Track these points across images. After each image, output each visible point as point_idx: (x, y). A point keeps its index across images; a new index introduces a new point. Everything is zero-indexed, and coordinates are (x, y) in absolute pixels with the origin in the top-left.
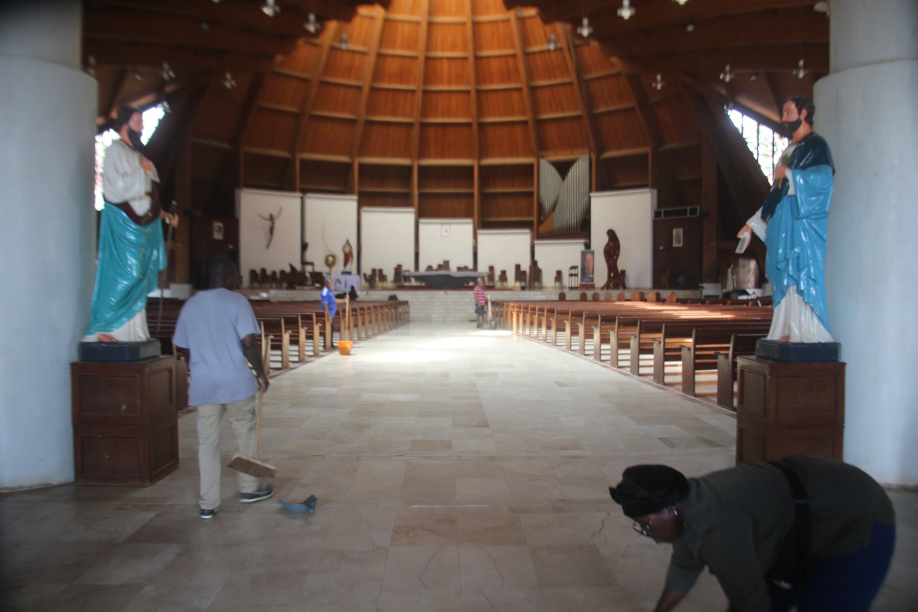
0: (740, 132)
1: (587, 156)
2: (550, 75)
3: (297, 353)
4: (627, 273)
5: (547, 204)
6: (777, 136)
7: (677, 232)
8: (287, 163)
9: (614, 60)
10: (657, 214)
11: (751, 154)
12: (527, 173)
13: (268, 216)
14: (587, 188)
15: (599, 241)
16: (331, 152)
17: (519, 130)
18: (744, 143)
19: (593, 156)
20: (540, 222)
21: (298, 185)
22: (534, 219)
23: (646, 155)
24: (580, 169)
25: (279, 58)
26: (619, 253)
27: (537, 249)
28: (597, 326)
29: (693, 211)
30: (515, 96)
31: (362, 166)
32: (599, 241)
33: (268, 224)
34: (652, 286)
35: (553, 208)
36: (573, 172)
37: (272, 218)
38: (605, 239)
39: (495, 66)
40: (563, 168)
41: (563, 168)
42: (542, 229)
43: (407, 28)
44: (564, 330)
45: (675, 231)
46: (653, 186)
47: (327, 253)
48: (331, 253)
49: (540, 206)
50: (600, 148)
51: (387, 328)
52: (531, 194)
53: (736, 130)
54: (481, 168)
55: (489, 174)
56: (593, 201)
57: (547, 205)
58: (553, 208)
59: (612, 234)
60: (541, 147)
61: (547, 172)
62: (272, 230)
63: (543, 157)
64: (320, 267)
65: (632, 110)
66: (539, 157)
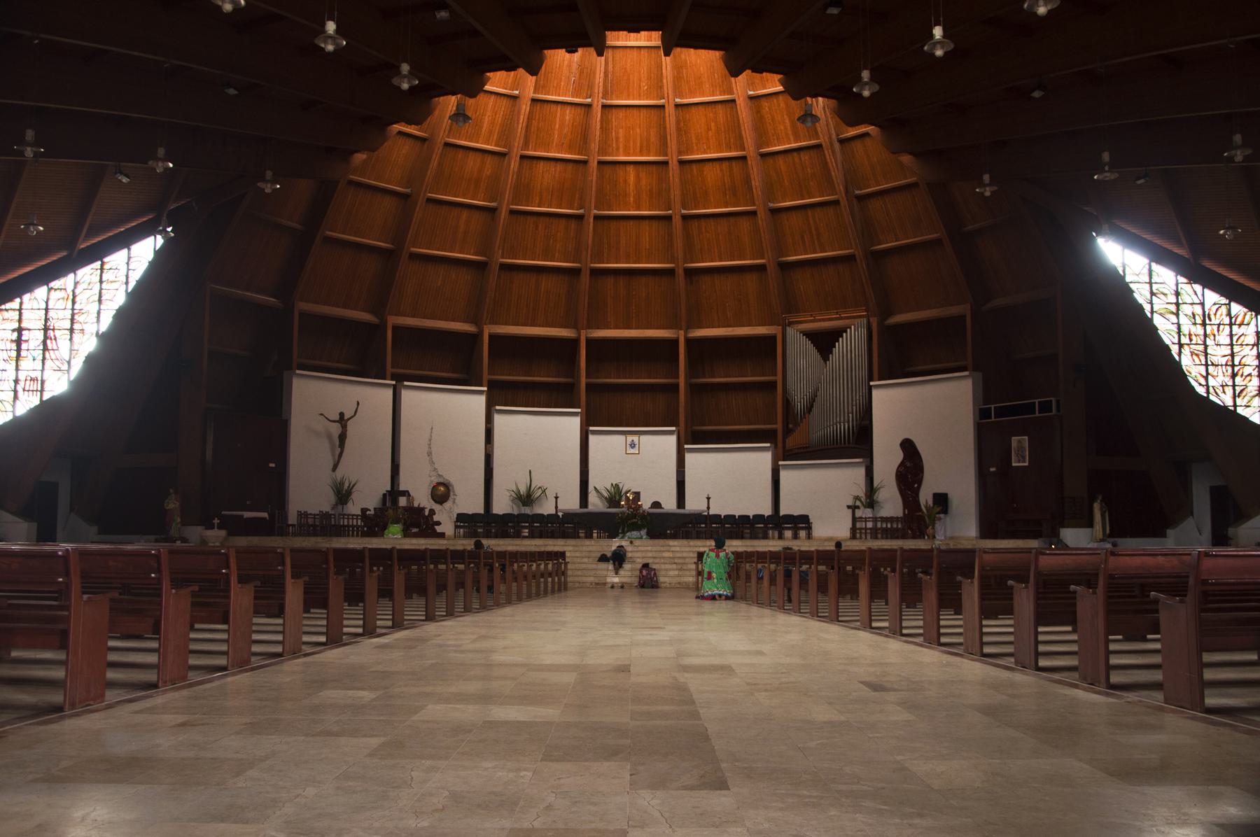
0: (1121, 273)
2: (802, 192)
3: (840, 604)
4: (949, 496)
5: (799, 400)
6: (1182, 279)
7: (1019, 441)
8: (375, 331)
9: (906, 159)
10: (982, 414)
11: (1141, 307)
12: (764, 349)
13: (337, 418)
14: (865, 373)
15: (887, 458)
16: (433, 317)
17: (751, 281)
18: (1125, 291)
19: (874, 321)
20: (787, 432)
21: (390, 370)
22: (779, 426)
23: (962, 318)
24: (852, 343)
25: (360, 157)
26: (922, 477)
27: (783, 474)
28: (1027, 582)
29: (1045, 407)
30: (745, 224)
31: (491, 336)
32: (887, 458)
33: (336, 429)
34: (978, 535)
35: (810, 409)
36: (841, 346)
37: (342, 420)
38: (899, 456)
39: (712, 175)
40: (824, 342)
41: (824, 342)
42: (790, 442)
43: (569, 113)
44: (1008, 611)
45: (1015, 439)
46: (975, 368)
47: (435, 480)
48: (441, 480)
49: (787, 403)
50: (886, 311)
51: (459, 606)
52: (772, 386)
53: (1115, 270)
54: (690, 342)
55: (703, 351)
56: (875, 393)
57: (799, 402)
59: (908, 447)
60: (789, 308)
61: (800, 351)
62: (343, 437)
63: (790, 324)
64: (422, 499)
65: (937, 242)
66: (785, 325)
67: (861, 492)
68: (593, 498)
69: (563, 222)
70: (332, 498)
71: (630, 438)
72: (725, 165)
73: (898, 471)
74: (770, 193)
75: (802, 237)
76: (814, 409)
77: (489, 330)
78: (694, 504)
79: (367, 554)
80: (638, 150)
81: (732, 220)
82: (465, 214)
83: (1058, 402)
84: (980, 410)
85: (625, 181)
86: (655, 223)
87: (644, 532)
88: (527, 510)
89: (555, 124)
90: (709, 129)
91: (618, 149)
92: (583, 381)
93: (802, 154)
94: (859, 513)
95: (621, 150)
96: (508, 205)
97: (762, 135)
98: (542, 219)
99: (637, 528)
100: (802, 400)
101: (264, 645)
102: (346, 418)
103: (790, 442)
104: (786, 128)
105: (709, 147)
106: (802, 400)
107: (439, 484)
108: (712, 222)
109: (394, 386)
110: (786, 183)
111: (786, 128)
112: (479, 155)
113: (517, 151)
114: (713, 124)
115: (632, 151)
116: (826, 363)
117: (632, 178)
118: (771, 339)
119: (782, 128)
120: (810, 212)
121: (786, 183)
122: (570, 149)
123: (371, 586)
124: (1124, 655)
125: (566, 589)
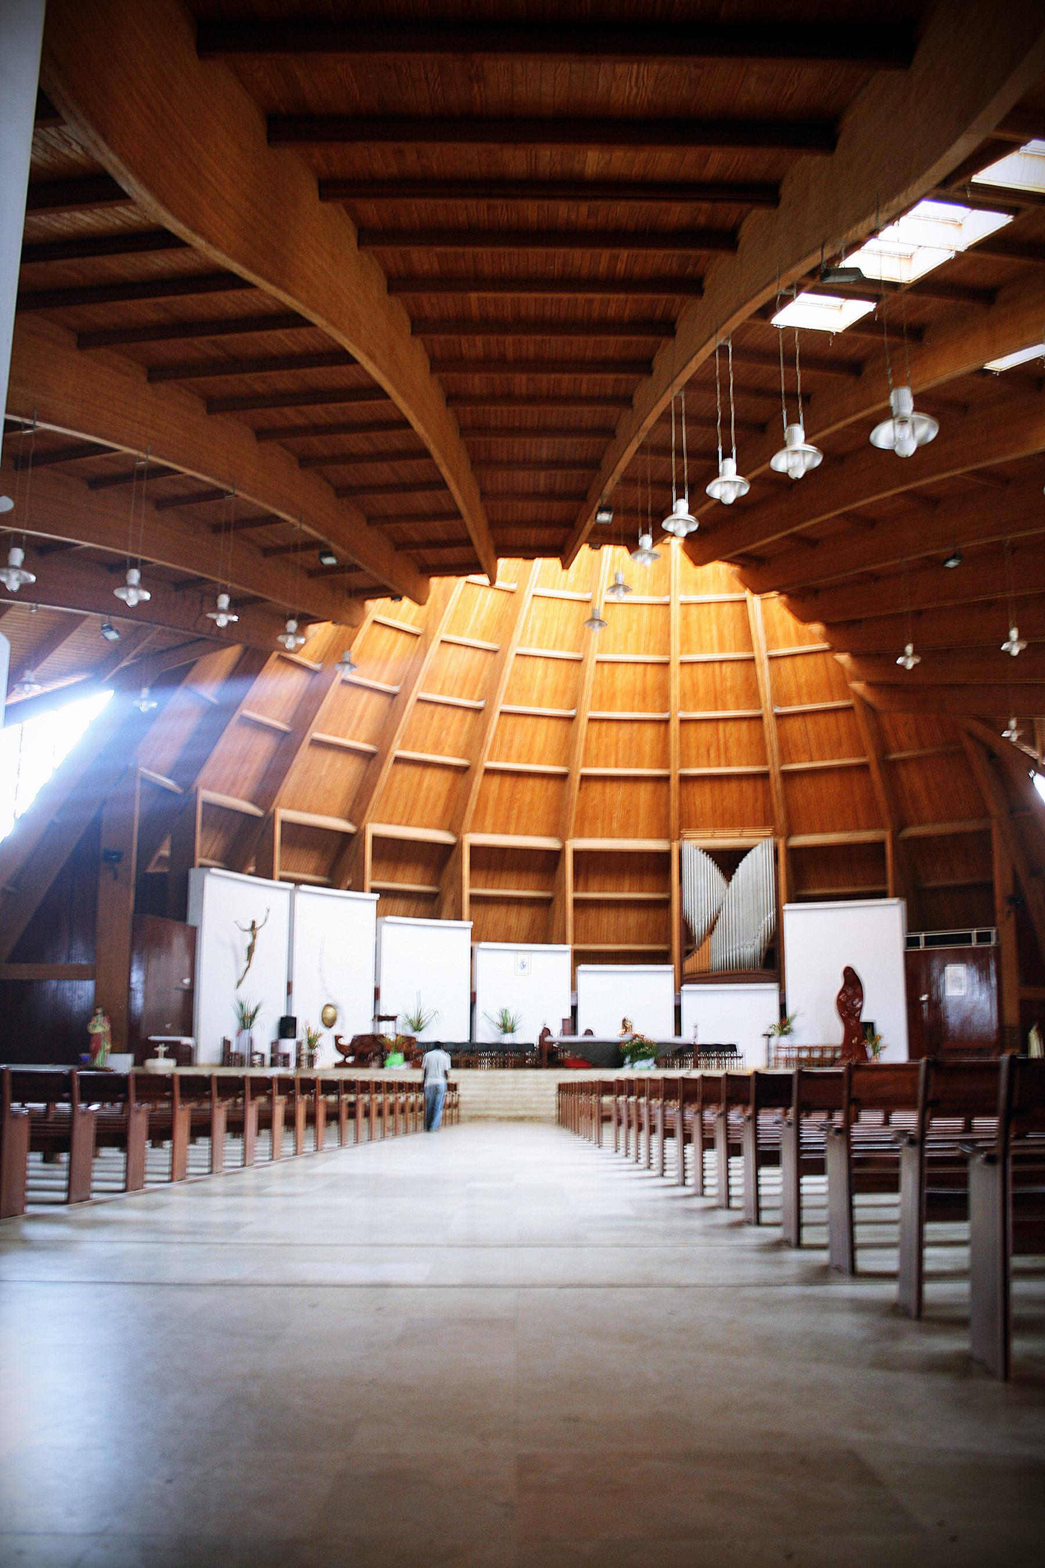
1: (770, 842)
13: (249, 926)
17: (644, 792)
20: (686, 953)
29: (983, 938)
31: (473, 848)
35: (711, 930)
42: (690, 965)
48: (329, 1002)
57: (699, 926)
58: (711, 930)
60: (687, 822)
62: (250, 950)
67: (775, 1019)
68: (481, 1023)
69: (460, 713)
70: (234, 1023)
71: (521, 957)
72: (641, 668)
73: (839, 1000)
74: (779, 698)
75: (708, 750)
76: (717, 931)
77: (374, 828)
78: (687, 1037)
79: (177, 1081)
80: (552, 643)
81: (636, 726)
82: (366, 695)
83: (997, 933)
84: (908, 938)
85: (532, 676)
86: (553, 722)
87: (651, 1061)
88: (508, 1039)
89: (474, 607)
90: (629, 629)
91: (531, 641)
92: (570, 895)
93: (724, 665)
94: (773, 1041)
95: (534, 643)
96: (417, 693)
97: (771, 641)
98: (439, 708)
99: (645, 1056)
100: (703, 920)
101: (101, 1189)
102: (257, 925)
103: (690, 965)
104: (711, 638)
105: (625, 648)
106: (703, 920)
107: (328, 1006)
108: (614, 727)
109: (291, 890)
110: (701, 693)
111: (711, 638)
112: (394, 633)
113: (768, 709)
114: (635, 626)
115: (545, 644)
116: (728, 885)
117: (539, 674)
118: (666, 855)
119: (708, 637)
120: (721, 726)
121: (701, 693)
122: (483, 637)
123: (139, 1123)
124: (36, 1200)
125: (458, 1122)
